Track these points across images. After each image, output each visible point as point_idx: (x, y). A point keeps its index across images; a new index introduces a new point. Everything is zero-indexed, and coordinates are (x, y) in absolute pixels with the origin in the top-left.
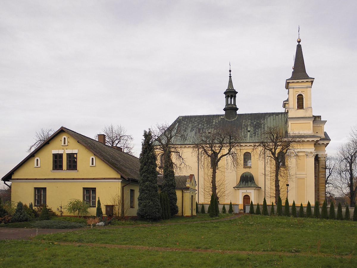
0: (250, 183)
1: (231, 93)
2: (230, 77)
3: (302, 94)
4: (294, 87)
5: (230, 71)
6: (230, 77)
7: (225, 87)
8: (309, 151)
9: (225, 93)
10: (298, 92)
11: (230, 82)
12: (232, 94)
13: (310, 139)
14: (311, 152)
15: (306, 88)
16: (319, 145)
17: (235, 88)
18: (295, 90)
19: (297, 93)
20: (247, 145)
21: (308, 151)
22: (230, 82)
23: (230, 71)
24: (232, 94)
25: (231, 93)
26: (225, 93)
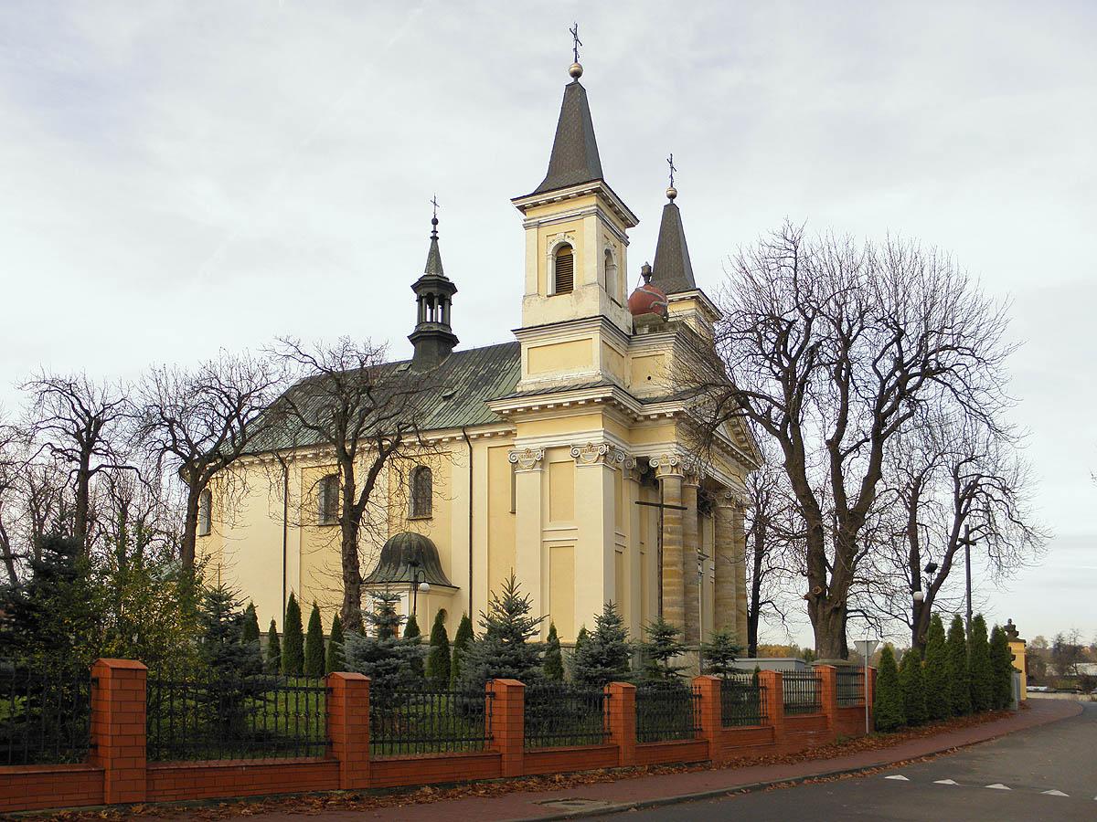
0: (404, 568)
1: (435, 290)
2: (435, 238)
3: (567, 240)
4: (542, 220)
5: (435, 222)
6: (435, 238)
7: (419, 272)
8: (582, 440)
9: (415, 287)
10: (554, 237)
11: (434, 255)
12: (431, 290)
13: (580, 397)
14: (591, 445)
15: (579, 217)
16: (648, 423)
17: (450, 272)
18: (545, 231)
19: (551, 239)
20: (482, 432)
21: (575, 442)
22: (434, 255)
23: (435, 222)
24: (431, 290)
25: (435, 290)
26: (415, 287)
